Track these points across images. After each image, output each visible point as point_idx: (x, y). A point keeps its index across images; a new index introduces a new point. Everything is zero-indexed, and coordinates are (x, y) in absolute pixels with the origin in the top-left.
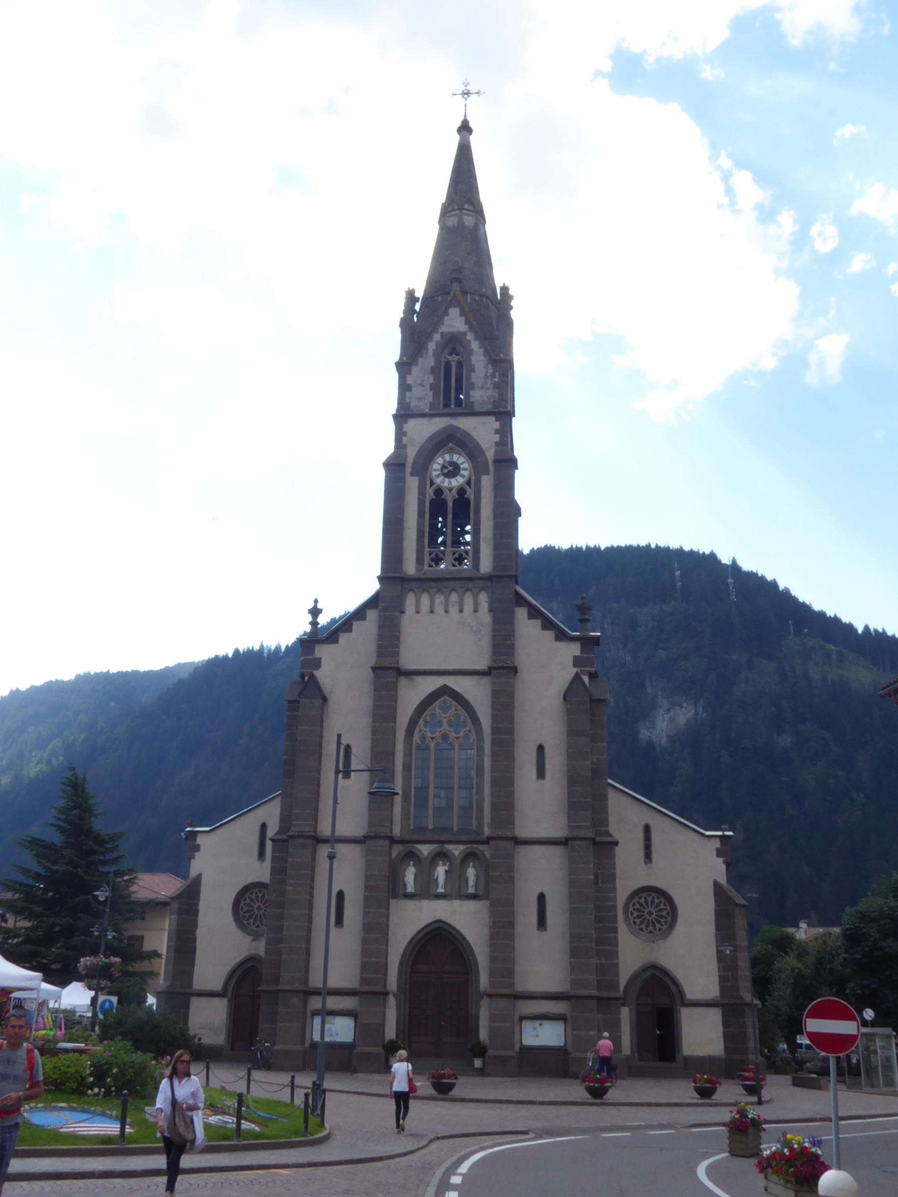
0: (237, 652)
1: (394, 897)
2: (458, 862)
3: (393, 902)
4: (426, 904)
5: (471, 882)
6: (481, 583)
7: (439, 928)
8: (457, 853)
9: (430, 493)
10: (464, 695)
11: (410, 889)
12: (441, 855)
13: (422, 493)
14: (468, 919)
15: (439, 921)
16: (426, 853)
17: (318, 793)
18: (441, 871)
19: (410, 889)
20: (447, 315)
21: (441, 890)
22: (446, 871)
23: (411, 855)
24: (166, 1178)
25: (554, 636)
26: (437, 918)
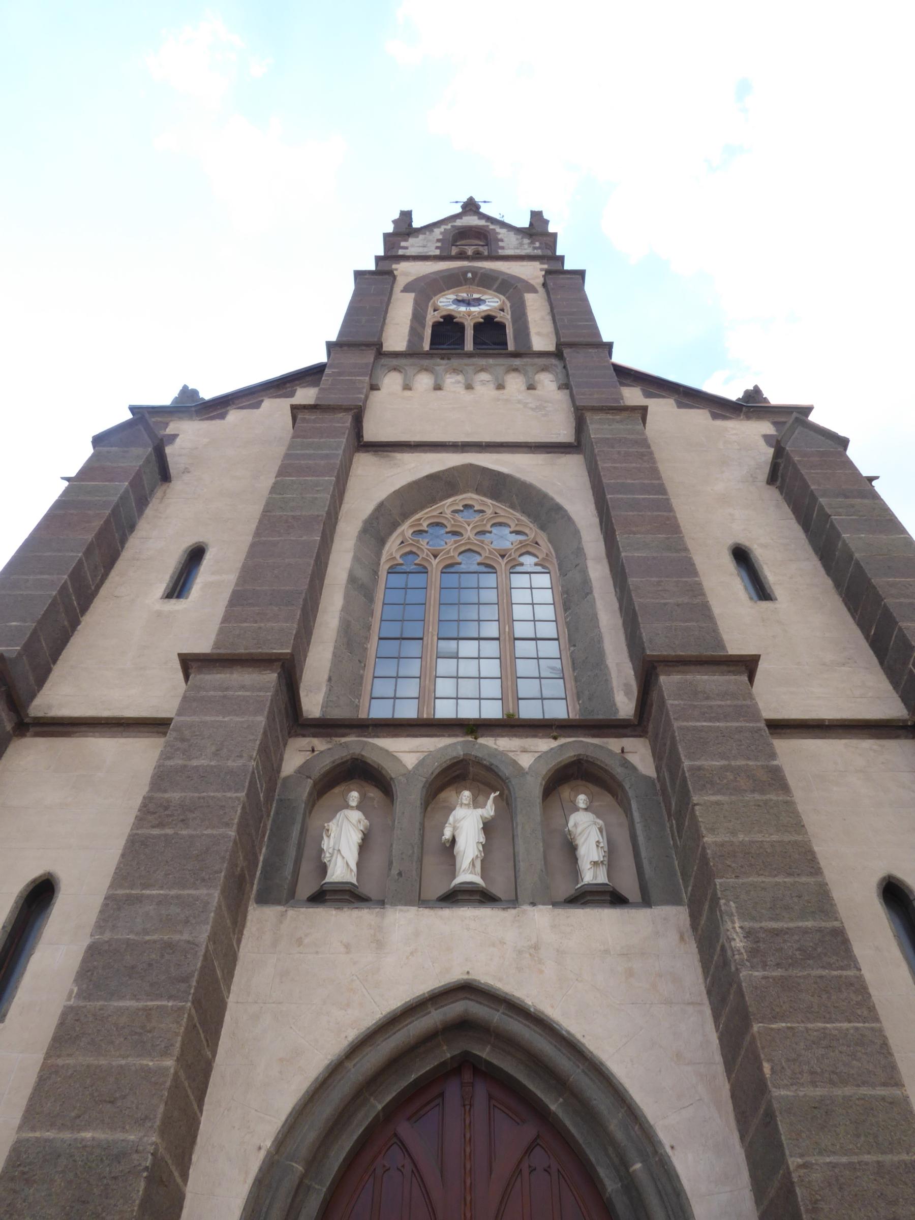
0: (395, 222)
4: (403, 921)
7: (463, 1026)
8: (526, 761)
10: (517, 475)
13: (418, 317)
15: (467, 989)
16: (410, 761)
18: (467, 822)
19: (342, 864)
20: (387, 236)
21: (467, 873)
22: (488, 827)
25: (708, 415)
26: (456, 975)
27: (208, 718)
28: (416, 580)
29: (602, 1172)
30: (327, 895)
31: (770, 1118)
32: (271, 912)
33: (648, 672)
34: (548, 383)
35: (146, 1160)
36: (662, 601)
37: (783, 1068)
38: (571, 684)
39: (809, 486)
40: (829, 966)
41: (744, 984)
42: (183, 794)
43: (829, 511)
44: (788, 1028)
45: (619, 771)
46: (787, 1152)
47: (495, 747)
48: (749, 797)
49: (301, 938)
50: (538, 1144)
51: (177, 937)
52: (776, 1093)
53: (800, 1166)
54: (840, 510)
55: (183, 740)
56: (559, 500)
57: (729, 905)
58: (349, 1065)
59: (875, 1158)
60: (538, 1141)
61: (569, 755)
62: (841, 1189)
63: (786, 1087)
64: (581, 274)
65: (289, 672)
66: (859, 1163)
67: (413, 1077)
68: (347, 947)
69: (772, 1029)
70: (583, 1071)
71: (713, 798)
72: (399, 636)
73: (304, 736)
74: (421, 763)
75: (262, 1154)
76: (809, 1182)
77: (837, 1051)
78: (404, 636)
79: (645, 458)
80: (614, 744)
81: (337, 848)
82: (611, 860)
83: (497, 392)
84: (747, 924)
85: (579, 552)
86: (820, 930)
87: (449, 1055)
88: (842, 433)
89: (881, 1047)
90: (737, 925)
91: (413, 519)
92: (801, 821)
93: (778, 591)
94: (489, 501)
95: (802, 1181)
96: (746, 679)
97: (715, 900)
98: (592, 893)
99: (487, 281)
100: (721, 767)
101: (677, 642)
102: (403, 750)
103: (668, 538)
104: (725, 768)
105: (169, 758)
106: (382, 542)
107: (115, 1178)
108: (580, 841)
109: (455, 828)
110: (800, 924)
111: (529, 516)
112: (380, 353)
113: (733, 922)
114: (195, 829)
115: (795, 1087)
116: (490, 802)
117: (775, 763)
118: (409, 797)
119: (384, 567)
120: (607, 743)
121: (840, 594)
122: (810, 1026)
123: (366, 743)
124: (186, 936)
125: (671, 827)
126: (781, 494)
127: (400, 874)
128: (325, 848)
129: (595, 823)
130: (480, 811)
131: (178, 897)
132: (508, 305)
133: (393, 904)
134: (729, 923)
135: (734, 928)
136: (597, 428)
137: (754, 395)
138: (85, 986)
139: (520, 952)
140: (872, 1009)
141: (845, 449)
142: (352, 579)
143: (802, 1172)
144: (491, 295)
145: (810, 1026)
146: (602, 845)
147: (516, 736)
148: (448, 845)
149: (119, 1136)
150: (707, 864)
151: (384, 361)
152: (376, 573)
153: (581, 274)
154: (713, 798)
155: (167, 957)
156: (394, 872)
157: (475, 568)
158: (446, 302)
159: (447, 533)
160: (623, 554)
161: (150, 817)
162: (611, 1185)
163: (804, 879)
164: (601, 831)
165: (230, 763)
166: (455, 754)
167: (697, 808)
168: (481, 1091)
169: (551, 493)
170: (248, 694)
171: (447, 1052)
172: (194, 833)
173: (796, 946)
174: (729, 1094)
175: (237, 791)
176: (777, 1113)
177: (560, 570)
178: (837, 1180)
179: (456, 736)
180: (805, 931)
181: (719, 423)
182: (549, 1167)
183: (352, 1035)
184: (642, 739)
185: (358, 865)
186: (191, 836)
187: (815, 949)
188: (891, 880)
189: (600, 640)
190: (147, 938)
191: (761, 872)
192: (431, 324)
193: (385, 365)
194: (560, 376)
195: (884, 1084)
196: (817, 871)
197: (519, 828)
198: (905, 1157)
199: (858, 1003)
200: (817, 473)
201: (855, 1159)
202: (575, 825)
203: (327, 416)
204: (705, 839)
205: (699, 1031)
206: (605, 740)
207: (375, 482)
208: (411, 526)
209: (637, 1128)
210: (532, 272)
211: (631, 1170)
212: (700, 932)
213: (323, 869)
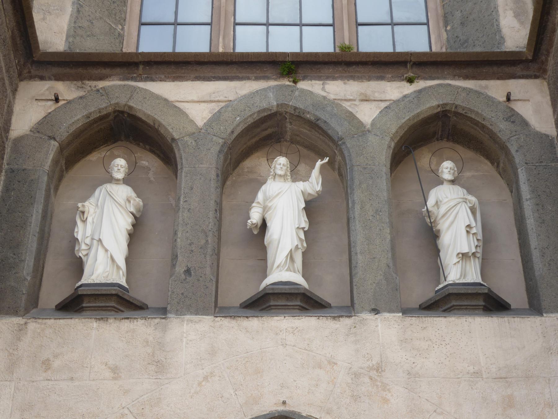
4: (193, 336)
8: (367, 114)
16: (200, 115)
18: (282, 200)
22: (311, 207)
45: (502, 128)
49: (48, 360)
61: (430, 104)
68: (115, 370)
74: (216, 118)
80: (496, 89)
81: (96, 237)
82: (486, 250)
102: (190, 98)
108: (443, 226)
109: (265, 209)
116: (316, 172)
118: (200, 166)
120: (486, 87)
123: (135, 88)
127: (188, 272)
128: (79, 238)
129: (465, 201)
130: (301, 185)
133: (179, 313)
146: (474, 231)
148: (255, 232)
156: (180, 269)
166: (265, 105)
184: (537, 81)
185: (128, 260)
197: (357, 207)
202: (437, 204)
206: (484, 83)
213: (78, 266)
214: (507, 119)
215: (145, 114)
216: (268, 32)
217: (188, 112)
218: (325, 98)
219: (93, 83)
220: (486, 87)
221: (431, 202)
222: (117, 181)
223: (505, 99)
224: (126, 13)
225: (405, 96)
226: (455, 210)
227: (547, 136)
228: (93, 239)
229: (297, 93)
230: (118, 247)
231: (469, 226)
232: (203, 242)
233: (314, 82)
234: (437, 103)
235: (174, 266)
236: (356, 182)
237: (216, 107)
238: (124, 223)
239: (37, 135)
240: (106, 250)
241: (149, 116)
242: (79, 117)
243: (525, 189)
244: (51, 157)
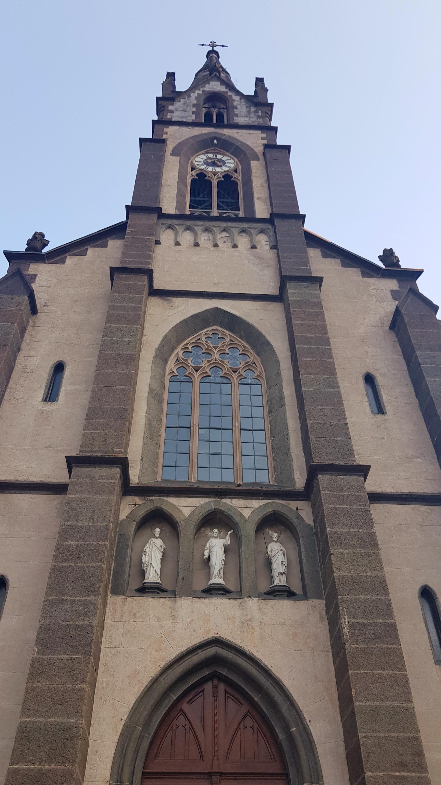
1: (115, 592)
2: (248, 530)
3: (115, 601)
4: (186, 606)
5: (278, 566)
6: (260, 226)
7: (215, 660)
8: (247, 513)
9: (190, 175)
10: (245, 318)
11: (153, 576)
12: (214, 520)
14: (280, 638)
15: (217, 642)
16: (187, 512)
17: (177, 121)
18: (216, 546)
21: (217, 579)
22: (226, 550)
23: (158, 518)
24: (151, 137)
25: (360, 273)
26: (211, 635)
27: (84, 496)
28: (186, 387)
29: (277, 730)
30: (146, 590)
31: (353, 713)
32: (119, 599)
33: (313, 471)
34: (263, 240)
35: (80, 731)
36: (323, 422)
37: (360, 692)
38: (271, 461)
39: (411, 342)
40: (386, 643)
41: (347, 651)
42: (77, 543)
43: (420, 361)
44: (365, 673)
45: (295, 521)
46: (359, 731)
47: (231, 504)
48: (358, 550)
49: (135, 613)
50: (248, 715)
51: (82, 623)
52: (356, 704)
53: (363, 737)
54: (427, 360)
55: (73, 509)
56: (269, 338)
57: (343, 610)
58: (161, 679)
59: (396, 735)
60: (248, 714)
61: (269, 510)
62: (380, 748)
63: (361, 701)
64: (288, 148)
65: (123, 464)
66: (389, 737)
67: (190, 684)
68: (158, 618)
69: (357, 673)
70: (271, 683)
71: (341, 551)
72: (177, 426)
73: (130, 495)
74: (193, 512)
75: (123, 722)
76: (367, 744)
77: (385, 685)
78: (180, 426)
79: (320, 317)
80: (293, 504)
81: (150, 562)
82: (288, 573)
83: (233, 249)
84: (351, 620)
85: (279, 375)
86: (384, 624)
87: (207, 673)
88: (435, 303)
89: (405, 683)
90: (346, 621)
91: (183, 344)
92: (382, 565)
93: (388, 407)
94: (227, 332)
95: (364, 744)
96: (363, 478)
97: (337, 606)
98: (279, 591)
99: (227, 146)
100: (346, 533)
101: (329, 450)
102: (183, 505)
103: (328, 378)
104: (347, 533)
105: (67, 521)
106: (166, 361)
107: (67, 739)
108: (273, 560)
109: (210, 551)
110: (376, 621)
111: (250, 345)
112: (162, 216)
113: (345, 619)
114: (85, 563)
115: (365, 701)
116: (228, 536)
117: (373, 530)
118: (187, 531)
119: (167, 378)
120: (289, 504)
121: (421, 410)
122: (375, 672)
123: (164, 500)
124: (86, 622)
125: (319, 556)
126: (397, 337)
127: (183, 579)
128: (144, 562)
129: (281, 550)
130: (223, 541)
131: (81, 601)
132: (240, 167)
133: (180, 596)
134: (343, 620)
135: (345, 622)
136: (294, 292)
137: (388, 256)
138: (40, 648)
139: (243, 623)
140: (404, 665)
141: (436, 314)
142: (151, 391)
143: (364, 740)
144: (228, 156)
145: (375, 672)
146: (284, 563)
147: (242, 498)
148: (206, 560)
149: (66, 720)
150: (335, 587)
151: (162, 221)
152: (163, 383)
153: (288, 148)
154: (341, 551)
155: (79, 633)
156: (180, 577)
157: (219, 380)
158: (199, 160)
159: (203, 353)
160: (303, 389)
161: (61, 556)
162: (281, 736)
163: (380, 597)
164: (284, 555)
165: (99, 524)
166: (210, 509)
167: (332, 556)
168: (222, 687)
169: (264, 333)
170: (105, 481)
171: (206, 672)
172: (84, 565)
173: (373, 632)
174: (337, 696)
175: (104, 541)
176: (356, 713)
177: (267, 384)
178: (379, 744)
179: (211, 497)
180: (378, 624)
181: (365, 279)
182: (253, 726)
183: (162, 664)
184: (307, 502)
185: (161, 570)
186: (83, 567)
187: (381, 634)
188: (426, 587)
189: (288, 438)
190: (67, 623)
191: (360, 593)
192: (190, 181)
193: (164, 224)
194: (272, 239)
195: (405, 701)
196: (386, 592)
197: (243, 553)
198: (409, 735)
199: (397, 662)
200: (417, 332)
201: (387, 735)
202: (271, 551)
203: (133, 277)
204: (335, 574)
205: (325, 664)
206: (288, 502)
207: (161, 319)
208: (182, 349)
209: (294, 711)
210: (254, 140)
211: (291, 730)
212: (329, 616)
213: (143, 574)
214: (297, 518)
215: (167, 511)
216: (210, 471)
217: (182, 510)
218: (231, 506)
219: (149, 497)
220: (289, 504)
221: (269, 550)
222: (157, 538)
223: (296, 509)
224: (158, 462)
225: (260, 506)
226: (278, 551)
227: (310, 525)
228: (148, 563)
229: (222, 504)
230: (157, 565)
231: (282, 561)
232: (188, 566)
233: (227, 499)
234: (272, 510)
235: (178, 576)
236: (243, 542)
237: (193, 509)
238: (159, 556)
239: (129, 519)
240: (154, 568)
241: (168, 512)
242: (143, 512)
243: (302, 547)
244: (134, 528)
